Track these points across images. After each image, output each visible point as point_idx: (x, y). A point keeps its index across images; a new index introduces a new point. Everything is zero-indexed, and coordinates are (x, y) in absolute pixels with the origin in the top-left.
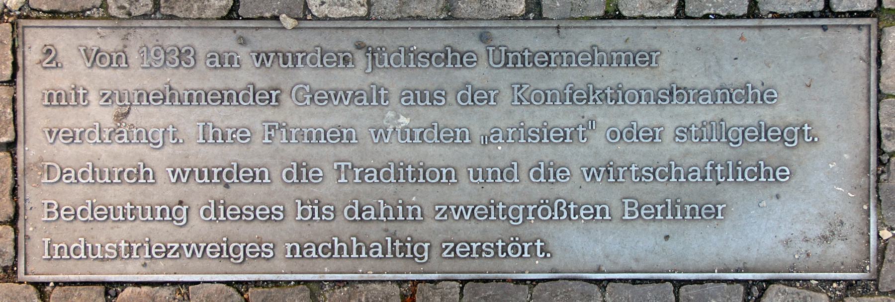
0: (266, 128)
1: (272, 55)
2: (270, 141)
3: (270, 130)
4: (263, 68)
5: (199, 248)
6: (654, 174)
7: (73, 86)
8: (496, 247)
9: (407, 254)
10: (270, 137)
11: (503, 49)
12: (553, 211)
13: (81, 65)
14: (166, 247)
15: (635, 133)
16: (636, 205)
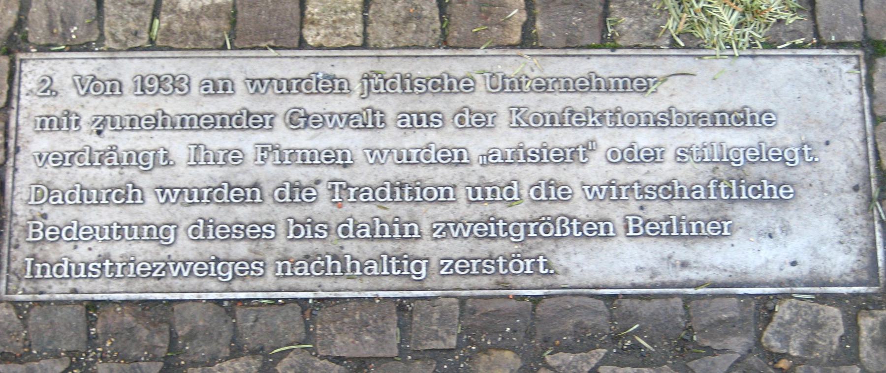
0: (259, 150)
1: (266, 82)
2: (263, 162)
3: (263, 152)
4: (257, 94)
6: (657, 192)
7: (66, 113)
8: (103, 267)
9: (471, 271)
10: (263, 159)
11: (500, 75)
12: (555, 227)
15: (636, 153)
16: (41, 226)
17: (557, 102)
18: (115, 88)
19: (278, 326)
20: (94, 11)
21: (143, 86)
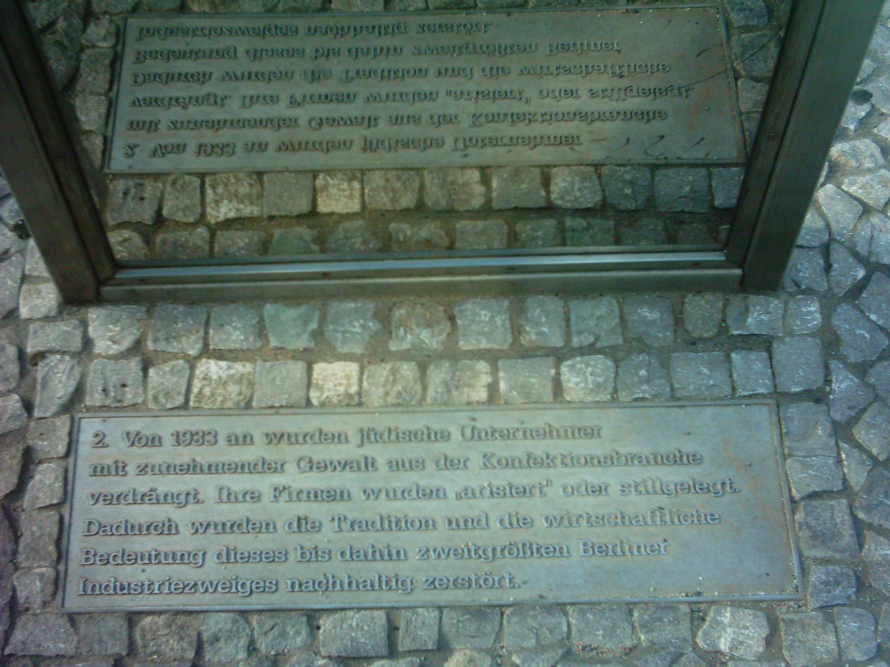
5: (211, 583)
13: (123, 444)
14: (183, 583)
17: (519, 448)
18: (155, 441)
19: (834, 570)
20: (141, 379)
21: (179, 438)
